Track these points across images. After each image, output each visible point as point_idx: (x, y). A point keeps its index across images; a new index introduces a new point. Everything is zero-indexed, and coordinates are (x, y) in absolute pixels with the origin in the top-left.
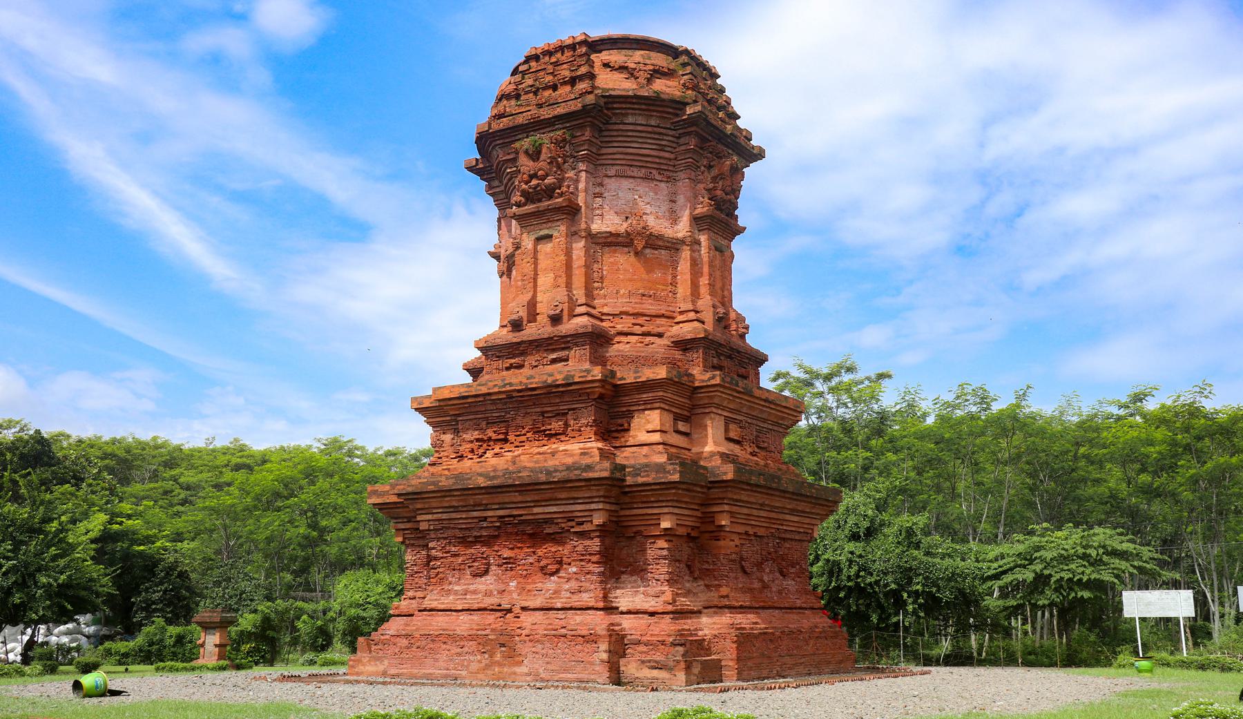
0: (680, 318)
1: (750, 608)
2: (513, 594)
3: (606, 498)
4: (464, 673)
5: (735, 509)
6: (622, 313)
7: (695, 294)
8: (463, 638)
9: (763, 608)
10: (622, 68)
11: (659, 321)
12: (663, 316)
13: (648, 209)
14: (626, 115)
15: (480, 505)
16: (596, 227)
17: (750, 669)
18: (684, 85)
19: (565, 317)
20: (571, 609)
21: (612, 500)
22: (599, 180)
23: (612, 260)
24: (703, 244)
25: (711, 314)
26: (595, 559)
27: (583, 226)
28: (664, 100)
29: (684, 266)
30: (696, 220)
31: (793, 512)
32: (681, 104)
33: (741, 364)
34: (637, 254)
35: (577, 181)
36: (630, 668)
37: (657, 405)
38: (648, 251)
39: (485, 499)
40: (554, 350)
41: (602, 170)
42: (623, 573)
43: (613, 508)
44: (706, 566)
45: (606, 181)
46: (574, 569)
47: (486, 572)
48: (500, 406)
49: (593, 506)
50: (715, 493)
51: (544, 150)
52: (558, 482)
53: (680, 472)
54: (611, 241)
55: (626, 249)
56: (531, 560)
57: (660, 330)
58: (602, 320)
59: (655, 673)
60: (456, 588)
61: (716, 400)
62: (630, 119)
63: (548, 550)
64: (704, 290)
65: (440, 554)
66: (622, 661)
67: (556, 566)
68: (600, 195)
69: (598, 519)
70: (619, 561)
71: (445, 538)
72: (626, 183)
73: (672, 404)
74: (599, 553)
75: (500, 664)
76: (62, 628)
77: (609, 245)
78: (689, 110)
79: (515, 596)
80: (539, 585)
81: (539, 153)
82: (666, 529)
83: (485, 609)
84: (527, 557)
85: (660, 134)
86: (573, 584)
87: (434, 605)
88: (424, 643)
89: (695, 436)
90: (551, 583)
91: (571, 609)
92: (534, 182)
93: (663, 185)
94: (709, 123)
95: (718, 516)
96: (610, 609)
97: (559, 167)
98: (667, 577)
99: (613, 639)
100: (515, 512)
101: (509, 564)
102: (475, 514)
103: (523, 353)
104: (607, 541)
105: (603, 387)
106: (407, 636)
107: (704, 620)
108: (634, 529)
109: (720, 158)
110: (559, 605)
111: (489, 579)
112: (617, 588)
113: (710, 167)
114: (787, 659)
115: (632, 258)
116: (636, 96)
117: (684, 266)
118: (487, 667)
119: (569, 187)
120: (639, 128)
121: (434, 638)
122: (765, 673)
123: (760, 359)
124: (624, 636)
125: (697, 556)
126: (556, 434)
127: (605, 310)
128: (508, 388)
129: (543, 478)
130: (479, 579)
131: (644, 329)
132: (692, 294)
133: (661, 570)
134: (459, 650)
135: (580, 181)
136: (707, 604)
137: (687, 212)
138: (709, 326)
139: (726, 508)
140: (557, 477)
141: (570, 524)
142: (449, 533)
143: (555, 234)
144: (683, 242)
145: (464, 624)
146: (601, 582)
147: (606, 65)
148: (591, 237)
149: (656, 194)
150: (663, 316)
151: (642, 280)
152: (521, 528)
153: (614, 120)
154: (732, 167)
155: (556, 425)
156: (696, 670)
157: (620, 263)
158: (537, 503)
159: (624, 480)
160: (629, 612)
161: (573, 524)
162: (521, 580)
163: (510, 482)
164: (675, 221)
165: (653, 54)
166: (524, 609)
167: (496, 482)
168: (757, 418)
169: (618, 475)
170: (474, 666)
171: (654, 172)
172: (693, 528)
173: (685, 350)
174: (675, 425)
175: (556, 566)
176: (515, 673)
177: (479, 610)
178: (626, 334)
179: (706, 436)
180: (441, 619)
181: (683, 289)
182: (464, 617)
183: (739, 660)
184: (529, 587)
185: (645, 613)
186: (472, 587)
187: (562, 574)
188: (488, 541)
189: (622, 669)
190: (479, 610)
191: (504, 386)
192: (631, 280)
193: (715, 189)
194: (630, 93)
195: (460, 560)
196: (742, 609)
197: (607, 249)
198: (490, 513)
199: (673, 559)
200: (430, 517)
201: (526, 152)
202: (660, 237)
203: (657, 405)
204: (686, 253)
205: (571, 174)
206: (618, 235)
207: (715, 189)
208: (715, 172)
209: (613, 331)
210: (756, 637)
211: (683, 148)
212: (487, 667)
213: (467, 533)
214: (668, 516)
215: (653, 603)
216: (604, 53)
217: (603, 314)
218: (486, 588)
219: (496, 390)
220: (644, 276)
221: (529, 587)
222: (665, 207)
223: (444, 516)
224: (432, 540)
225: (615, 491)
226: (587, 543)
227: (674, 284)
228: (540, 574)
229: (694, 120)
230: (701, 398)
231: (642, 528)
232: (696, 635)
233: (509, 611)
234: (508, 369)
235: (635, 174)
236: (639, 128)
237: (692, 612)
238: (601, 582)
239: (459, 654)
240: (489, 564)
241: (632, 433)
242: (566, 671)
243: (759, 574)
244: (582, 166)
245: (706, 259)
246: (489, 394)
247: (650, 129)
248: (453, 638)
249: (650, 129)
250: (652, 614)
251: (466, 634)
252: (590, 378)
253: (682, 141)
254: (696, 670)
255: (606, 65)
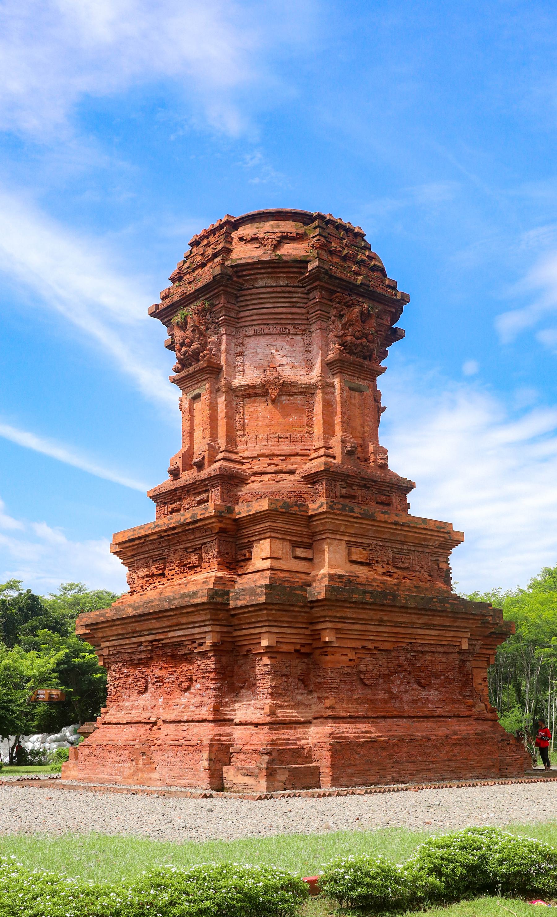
0: (314, 455)
1: (364, 717)
3: (215, 621)
4: (120, 778)
5: (340, 626)
6: (259, 455)
7: (329, 430)
9: (384, 717)
10: (254, 239)
11: (293, 459)
12: (297, 454)
13: (284, 361)
14: (256, 280)
15: (137, 632)
16: (238, 381)
17: (352, 775)
18: (313, 246)
19: (206, 464)
20: (192, 721)
21: (224, 623)
22: (240, 341)
23: (252, 409)
24: (337, 386)
25: (340, 448)
26: (212, 676)
27: (223, 382)
28: (287, 262)
29: (318, 408)
30: (328, 366)
31: (427, 626)
32: (303, 263)
33: (380, 492)
34: (273, 401)
35: (220, 343)
36: (230, 775)
37: (268, 535)
38: (284, 398)
39: (138, 627)
40: (200, 493)
41: (243, 332)
42: (242, 688)
43: (225, 629)
44: (319, 680)
45: (247, 340)
47: (146, 690)
48: (157, 545)
49: (206, 629)
50: (317, 612)
51: (189, 321)
52: (176, 609)
53: (266, 594)
54: (251, 393)
55: (264, 399)
57: (292, 468)
58: (243, 464)
59: (246, 780)
61: (328, 527)
62: (260, 283)
64: (338, 428)
66: (225, 769)
67: (187, 684)
68: (241, 354)
69: (209, 641)
70: (232, 679)
71: (120, 662)
72: (263, 340)
73: (286, 533)
74: (215, 670)
75: (143, 771)
76: (53, 737)
77: (249, 396)
78: (310, 267)
79: (161, 710)
81: (186, 323)
82: (267, 647)
85: (289, 292)
86: (198, 699)
88: (98, 752)
89: (316, 561)
90: (146, 699)
91: (192, 721)
92: (184, 349)
93: (299, 338)
94: (331, 276)
95: (323, 633)
96: (220, 720)
97: (201, 334)
98: (269, 691)
99: (215, 748)
100: (158, 637)
102: (134, 640)
103: (180, 499)
104: (224, 660)
105: (220, 521)
107: (312, 729)
108: (246, 648)
109: (349, 306)
110: (185, 719)
111: (147, 695)
112: (236, 702)
113: (341, 316)
114: (408, 766)
115: (270, 406)
116: (260, 262)
117: (318, 408)
118: (135, 772)
119: (211, 350)
120: (269, 290)
122: (372, 779)
123: (407, 487)
124: (228, 747)
125: (303, 668)
126: (195, 567)
127: (246, 454)
128: (157, 529)
129: (166, 606)
131: (279, 468)
132: (325, 433)
133: (265, 684)
135: (221, 343)
136: (317, 715)
137: (319, 359)
138: (338, 461)
139: (328, 625)
140: (176, 604)
142: (122, 656)
143: (203, 392)
144: (315, 386)
146: (216, 697)
147: (241, 239)
148: (230, 390)
149: (292, 346)
150: (297, 454)
151: (278, 424)
153: (246, 286)
154: (362, 313)
155: (194, 559)
156: (282, 776)
157: (259, 413)
158: (171, 628)
159: (229, 604)
160: (241, 724)
163: (147, 611)
164: (310, 369)
165: (281, 223)
166: (164, 721)
167: (139, 612)
168: (391, 541)
169: (219, 600)
170: (127, 772)
171: (289, 327)
172: (303, 645)
173: (313, 483)
174: (293, 551)
175: (187, 684)
176: (150, 779)
178: (261, 474)
179: (324, 559)
181: (318, 429)
182: (128, 730)
183: (333, 766)
184: (171, 702)
185: (251, 724)
187: (192, 690)
188: (146, 663)
189: (224, 775)
191: (154, 528)
192: (268, 426)
193: (345, 335)
194: (255, 260)
195: (130, 680)
196: (353, 719)
197: (247, 400)
198: (143, 639)
199: (276, 673)
200: (108, 644)
201: (177, 325)
202: (293, 384)
203: (268, 535)
204: (319, 396)
205: (214, 338)
206: (254, 387)
207: (345, 335)
208: (345, 320)
209: (250, 472)
210: (359, 745)
211: (312, 302)
212: (135, 773)
214: (266, 635)
215: (258, 715)
216: (240, 229)
217: (244, 458)
219: (149, 532)
220: (281, 420)
222: (301, 357)
223: (116, 643)
225: (222, 615)
226: (207, 661)
227: (310, 424)
229: (316, 275)
230: (317, 526)
231: (251, 647)
232: (295, 744)
234: (171, 513)
235: (271, 331)
236: (269, 290)
237: (299, 723)
238: (216, 697)
239: (118, 762)
240: (147, 683)
241: (253, 561)
242: (182, 776)
243: (385, 686)
244: (223, 330)
245: (339, 400)
246: (147, 536)
247: (279, 289)
248: (116, 747)
249: (279, 289)
250: (256, 725)
252: (207, 515)
253: (311, 296)
254: (282, 776)
255: (241, 239)
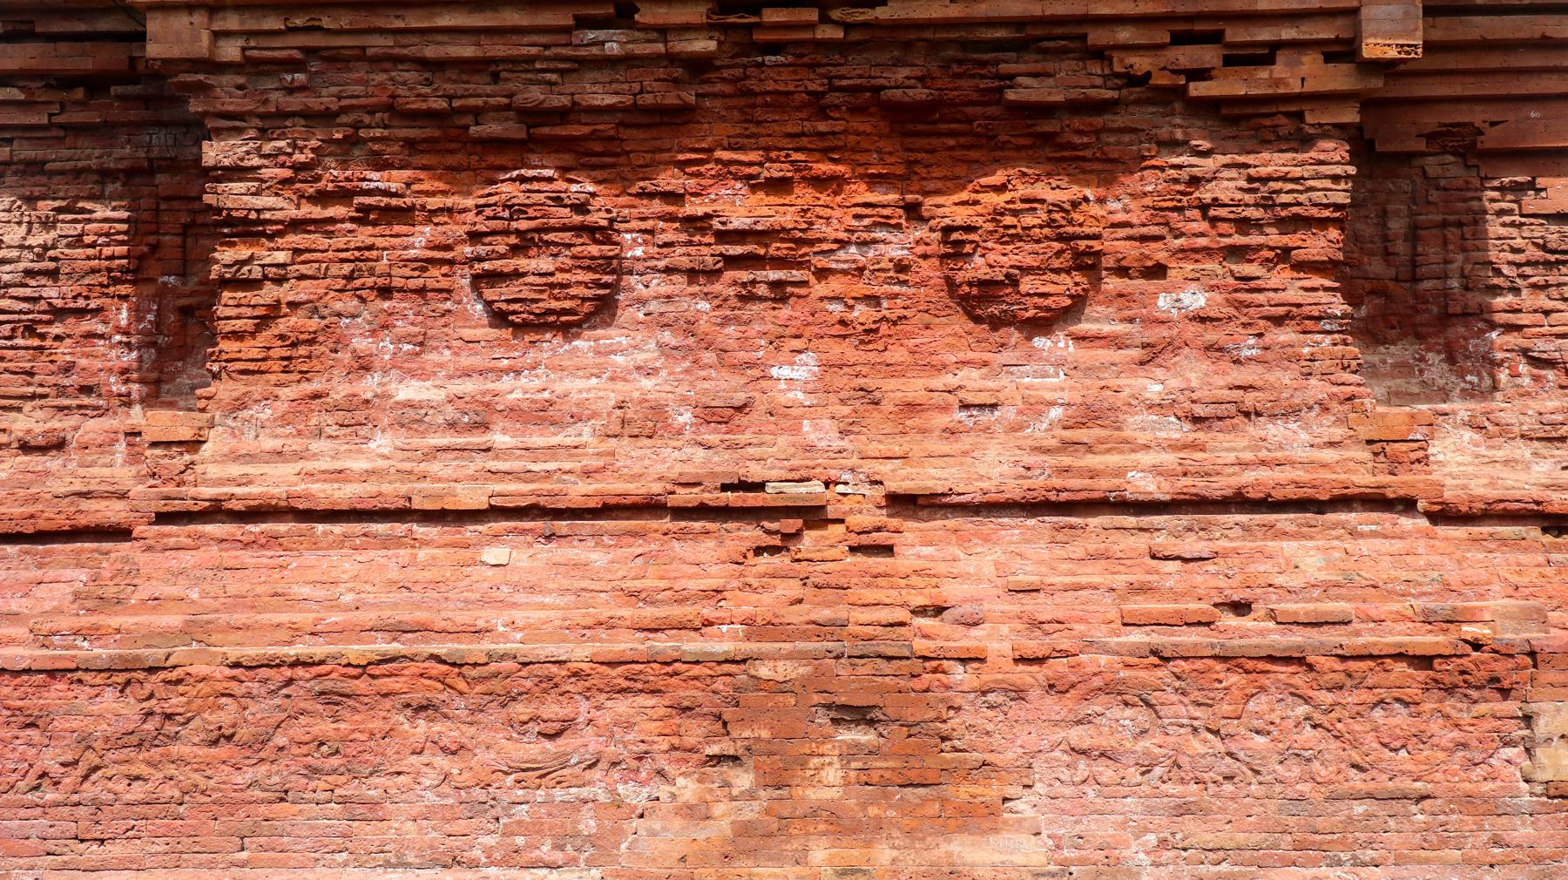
2: (800, 411)
8: (553, 678)
46: (1195, 299)
47: (603, 309)
56: (895, 247)
60: (408, 391)
63: (1004, 198)
65: (281, 206)
74: (1340, 218)
75: (836, 823)
79: (820, 433)
80: (970, 378)
83: (651, 507)
84: (864, 229)
87: (276, 481)
88: (263, 710)
91: (1239, 502)
101: (761, 266)
106: (125, 674)
108: (1431, 120)
121: (339, 686)
130: (551, 346)
134: (534, 749)
141: (1186, 56)
142: (360, 86)
145: (527, 597)
152: (853, 71)
161: (1208, 56)
162: (846, 350)
166: (904, 503)
177: (608, 510)
180: (345, 564)
184: (897, 390)
186: (514, 390)
190: (608, 510)
195: (420, 238)
213: (481, 92)
218: (619, 389)
221: (897, 390)
224: (233, 123)
228: (960, 323)
231: (1478, 116)
233: (814, 516)
248: (457, 680)
251: (579, 652)
